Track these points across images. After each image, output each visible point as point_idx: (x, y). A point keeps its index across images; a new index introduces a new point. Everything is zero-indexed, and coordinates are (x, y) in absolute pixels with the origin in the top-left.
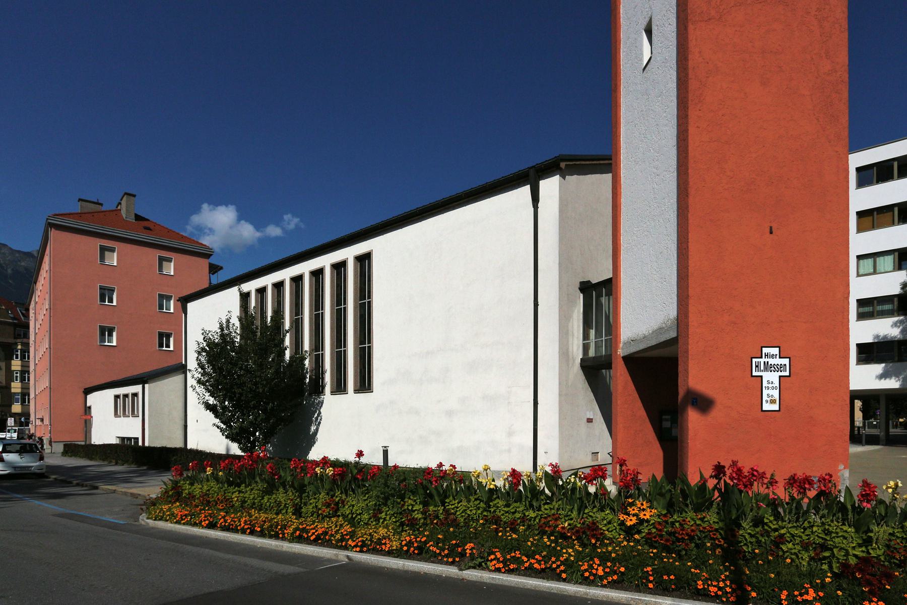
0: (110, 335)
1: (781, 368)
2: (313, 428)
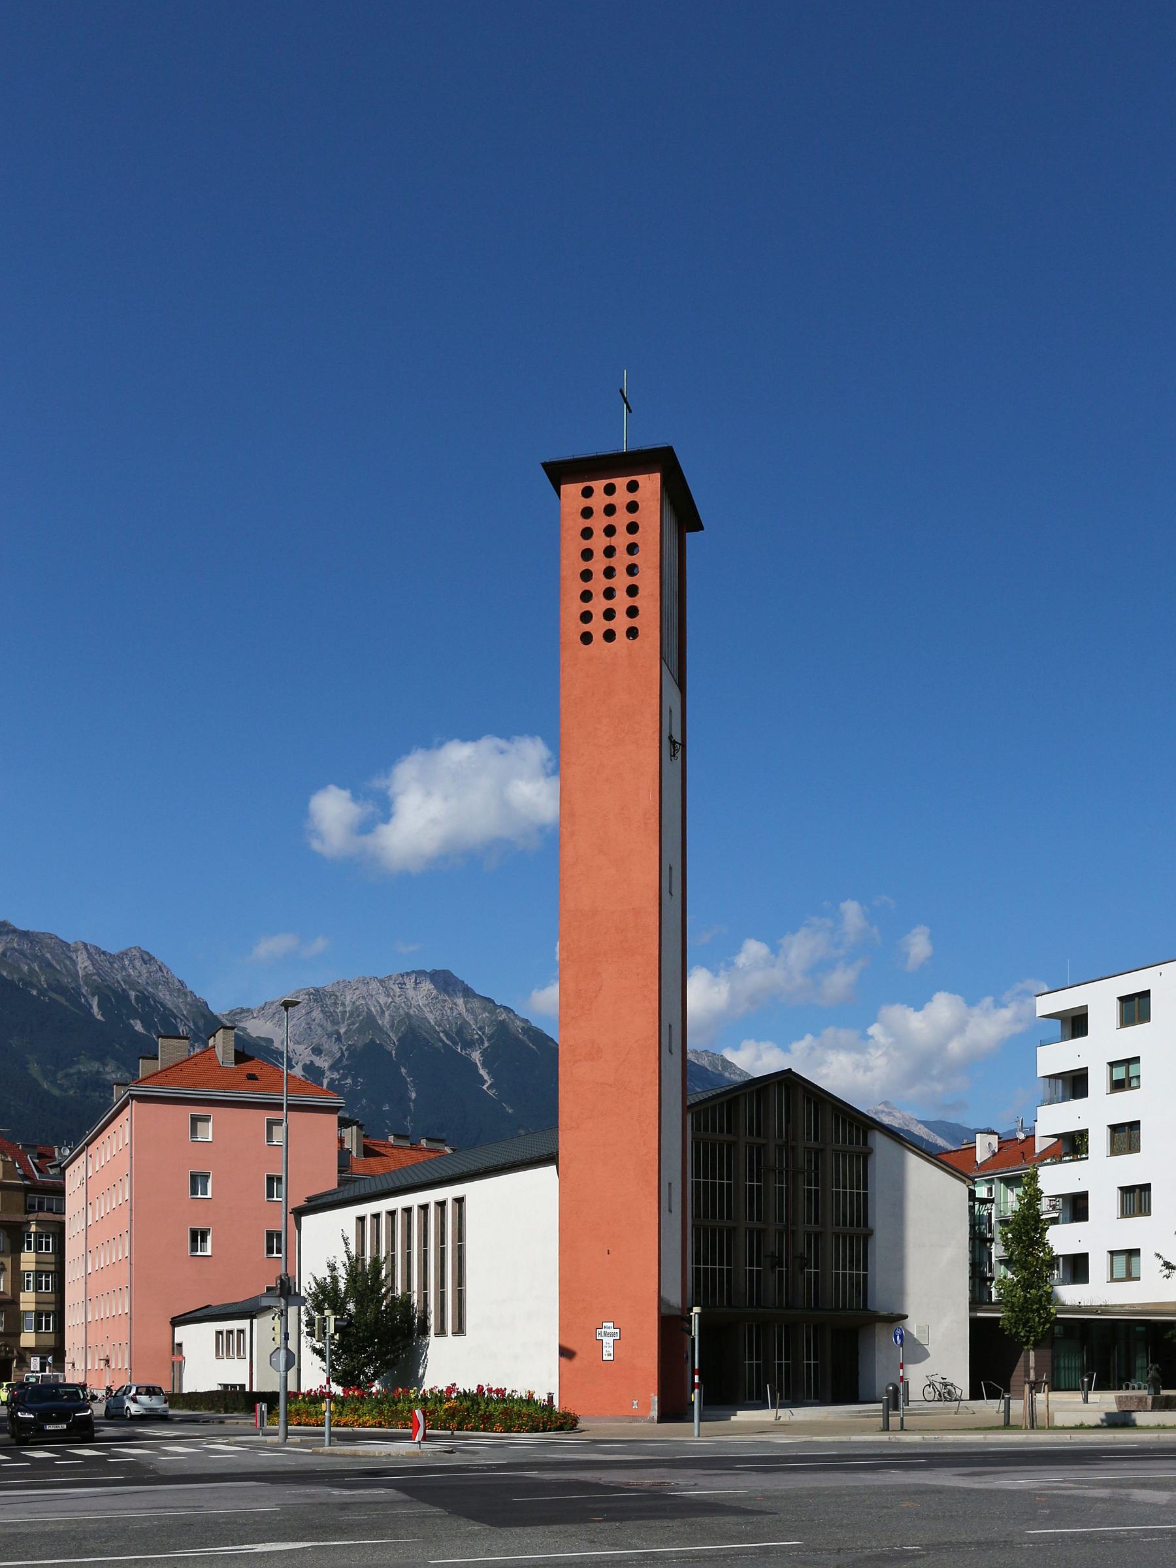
0: (204, 1240)
2: (421, 1371)
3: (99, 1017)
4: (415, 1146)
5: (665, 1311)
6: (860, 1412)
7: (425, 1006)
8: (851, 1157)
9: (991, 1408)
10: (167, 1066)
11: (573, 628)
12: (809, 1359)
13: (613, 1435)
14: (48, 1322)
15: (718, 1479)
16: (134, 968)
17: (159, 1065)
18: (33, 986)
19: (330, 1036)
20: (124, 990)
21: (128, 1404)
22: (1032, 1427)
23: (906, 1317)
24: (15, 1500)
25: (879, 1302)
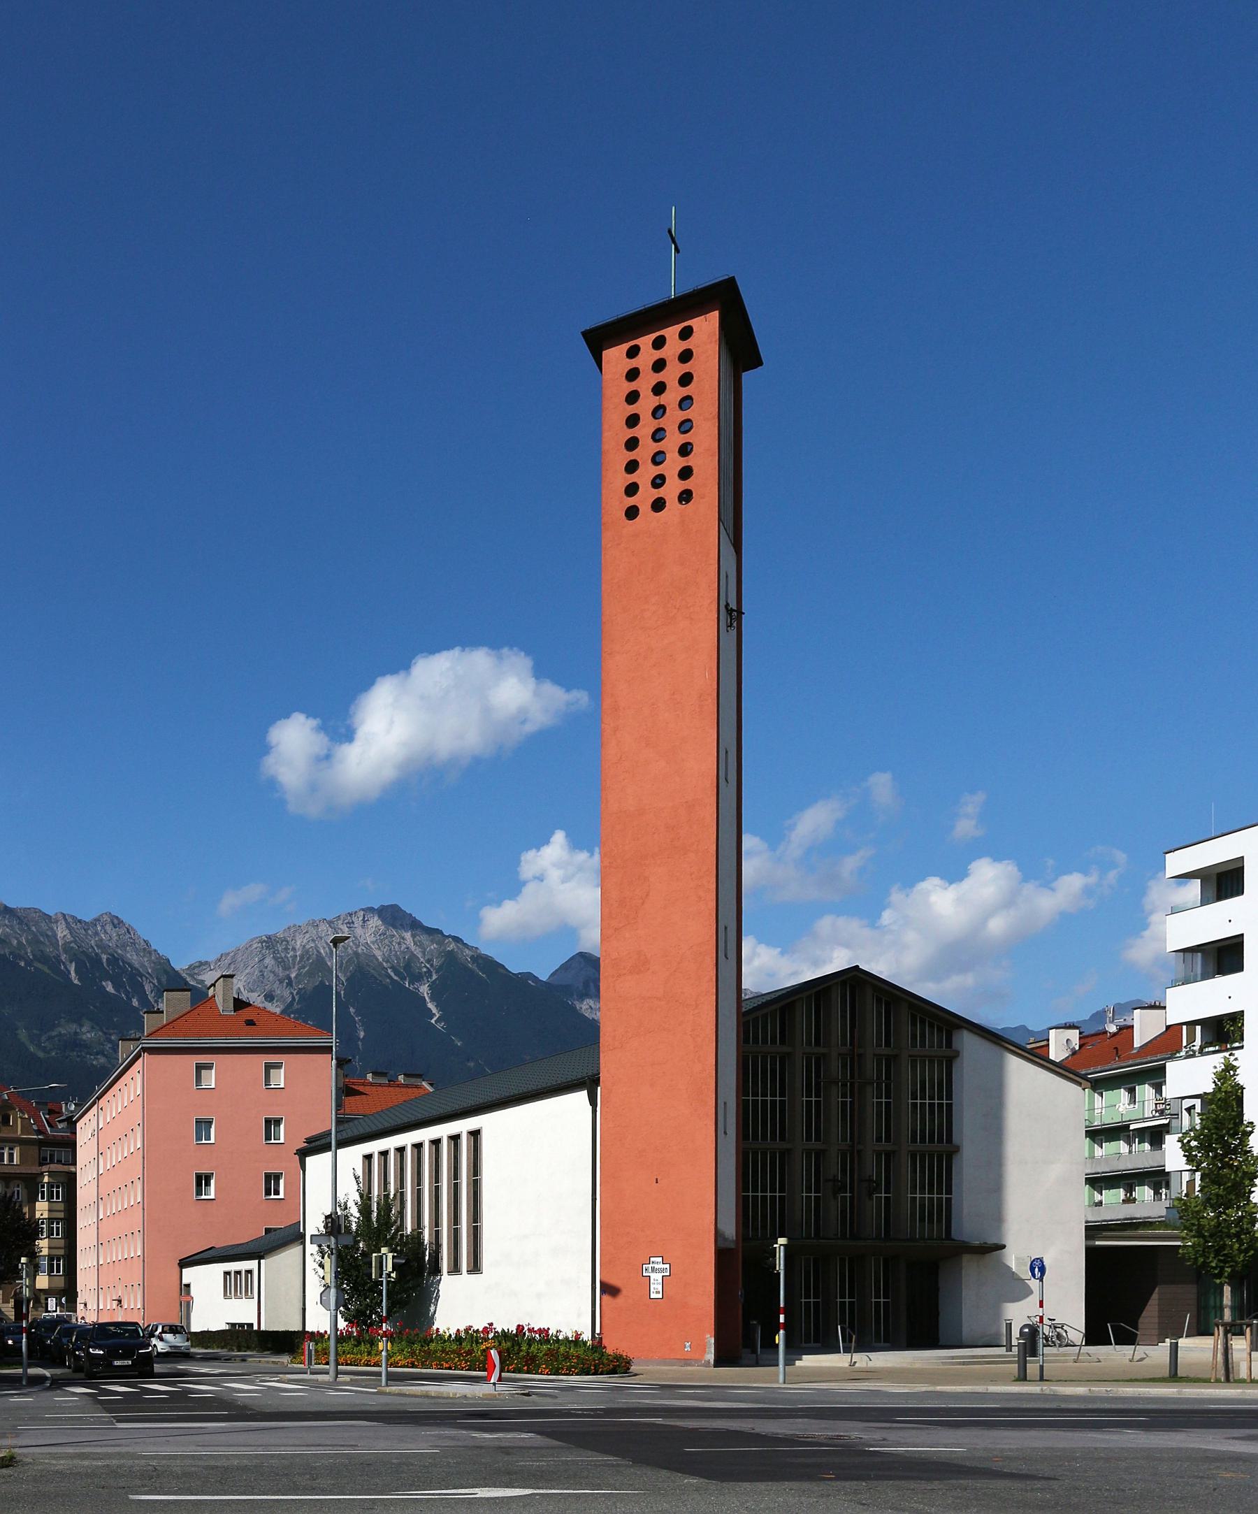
1: (662, 1270)
2: (432, 1308)
3: (76, 982)
4: (392, 1082)
5: (721, 1245)
6: (953, 1358)
7: (373, 943)
8: (932, 1062)
9: (1115, 1355)
10: (172, 1018)
11: (616, 502)
12: (808, 1296)
13: (673, 1379)
14: (58, 1266)
15: (901, 1433)
16: (106, 932)
17: (165, 1019)
18: (21, 958)
19: (281, 982)
20: (97, 954)
21: (154, 1341)
22: (1228, 1380)
23: (1004, 1247)
24: (182, 1432)
25: (967, 1227)
